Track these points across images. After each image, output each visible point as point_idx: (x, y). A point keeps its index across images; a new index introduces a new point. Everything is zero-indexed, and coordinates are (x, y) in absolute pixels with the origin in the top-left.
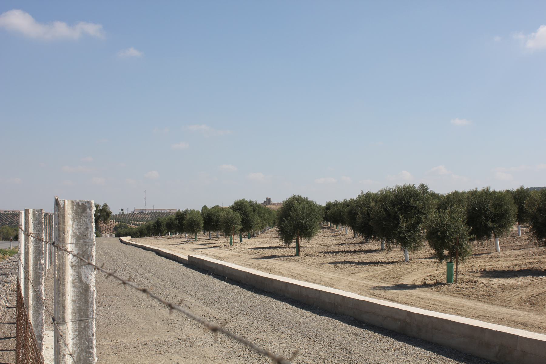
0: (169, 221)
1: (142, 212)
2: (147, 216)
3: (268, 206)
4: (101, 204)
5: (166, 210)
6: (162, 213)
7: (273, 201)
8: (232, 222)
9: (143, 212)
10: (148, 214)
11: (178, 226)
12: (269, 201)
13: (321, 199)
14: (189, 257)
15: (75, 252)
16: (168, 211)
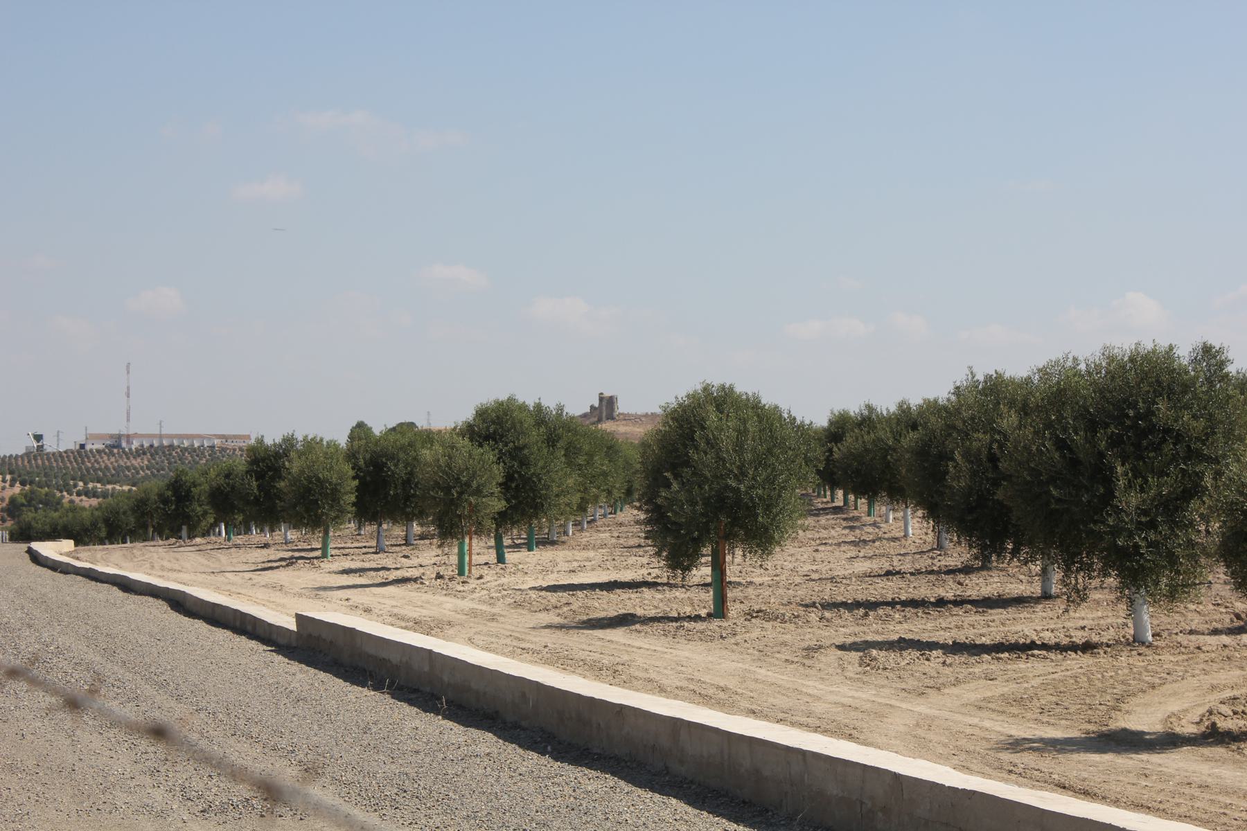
0: (221, 480)
1: (115, 444)
2: (136, 462)
3: (607, 426)
4: (607, 394)
5: (209, 437)
7: (622, 407)
9: (118, 446)
10: (141, 452)
14: (300, 618)
16: (217, 442)
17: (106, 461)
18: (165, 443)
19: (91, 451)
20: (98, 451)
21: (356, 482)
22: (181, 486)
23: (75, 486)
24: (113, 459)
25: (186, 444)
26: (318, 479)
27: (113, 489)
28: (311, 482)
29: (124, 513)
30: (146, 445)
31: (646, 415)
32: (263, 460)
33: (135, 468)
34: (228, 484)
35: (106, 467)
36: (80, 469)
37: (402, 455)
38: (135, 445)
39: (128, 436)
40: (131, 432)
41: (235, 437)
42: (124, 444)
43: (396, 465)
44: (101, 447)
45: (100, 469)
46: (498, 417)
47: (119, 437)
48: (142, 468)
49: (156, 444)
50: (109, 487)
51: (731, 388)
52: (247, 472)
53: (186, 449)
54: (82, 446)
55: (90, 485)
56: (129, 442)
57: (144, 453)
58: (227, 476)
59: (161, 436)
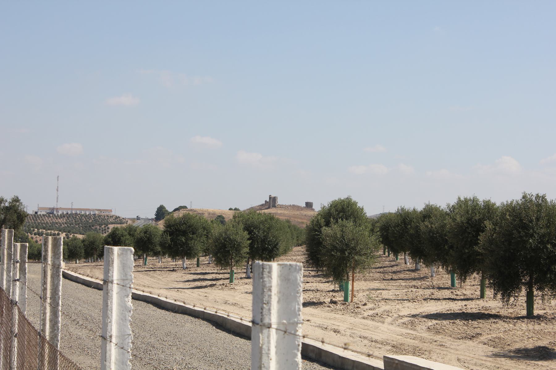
0: (142, 234)
1: (51, 212)
2: (60, 221)
3: (272, 211)
4: (273, 196)
5: (93, 210)
7: (280, 202)
8: (354, 249)
9: (53, 213)
10: (62, 216)
11: (170, 246)
12: (272, 202)
13: (377, 203)
14: (388, 362)
16: (97, 212)
17: (47, 220)
18: (74, 212)
19: (40, 215)
20: (43, 215)
21: (249, 242)
22: (116, 236)
23: (34, 230)
24: (50, 219)
25: (83, 213)
26: (230, 239)
27: (51, 232)
28: (225, 241)
29: (80, 247)
30: (65, 213)
32: (173, 226)
33: (60, 223)
34: (146, 237)
35: (47, 222)
36: (35, 223)
37: (261, 226)
38: (60, 213)
39: (57, 209)
40: (58, 207)
41: (105, 210)
42: (55, 212)
43: (258, 232)
44: (45, 213)
45: (44, 223)
46: (343, 208)
47: (53, 209)
48: (63, 223)
49: (69, 213)
50: (49, 231)
51: (543, 197)
52: (164, 232)
53: (83, 215)
54: (36, 213)
55: (40, 230)
57: (64, 217)
58: (145, 233)
59: (72, 209)
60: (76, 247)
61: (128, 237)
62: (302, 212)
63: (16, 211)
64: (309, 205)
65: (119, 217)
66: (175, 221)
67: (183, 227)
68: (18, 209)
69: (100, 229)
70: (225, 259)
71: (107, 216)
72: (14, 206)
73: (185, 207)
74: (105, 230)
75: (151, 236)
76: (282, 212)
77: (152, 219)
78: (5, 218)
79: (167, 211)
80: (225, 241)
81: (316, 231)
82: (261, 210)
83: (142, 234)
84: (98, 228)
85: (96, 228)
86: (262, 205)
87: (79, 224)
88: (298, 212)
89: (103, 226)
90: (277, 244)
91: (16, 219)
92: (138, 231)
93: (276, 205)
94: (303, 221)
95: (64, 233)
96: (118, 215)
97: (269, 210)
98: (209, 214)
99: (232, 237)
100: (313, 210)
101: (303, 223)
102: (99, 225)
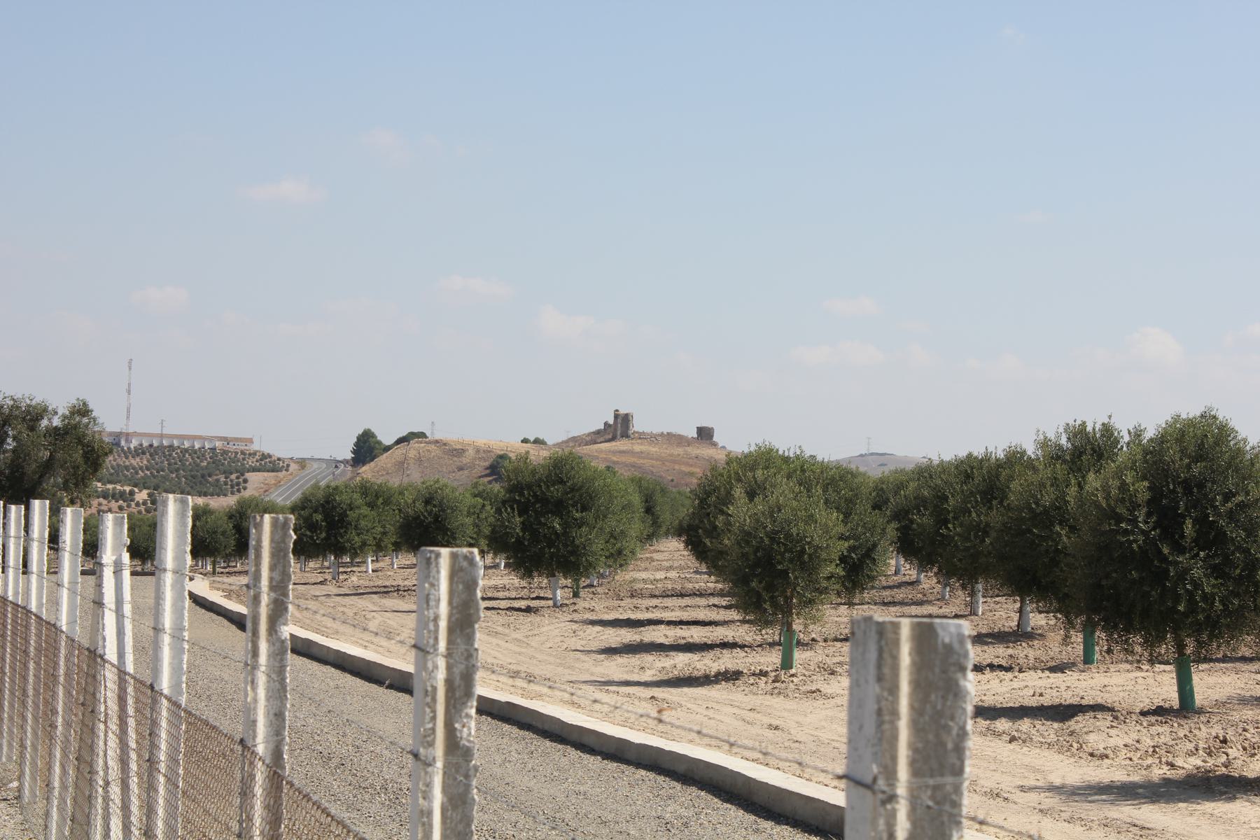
2: (135, 462)
4: (623, 411)
5: (211, 439)
6: (191, 451)
7: (638, 426)
9: (118, 444)
10: (140, 451)
11: (519, 541)
12: (620, 426)
15: (267, 761)
16: (218, 444)
18: (165, 443)
22: (334, 508)
25: (187, 445)
26: (788, 536)
29: (223, 533)
30: (145, 444)
31: (662, 434)
32: (529, 487)
34: (430, 513)
38: (134, 443)
39: (127, 434)
40: (131, 431)
42: (123, 443)
48: (141, 468)
49: (156, 444)
50: (110, 486)
53: (186, 450)
56: (127, 441)
57: (144, 453)
58: (428, 502)
59: (162, 436)
60: (215, 532)
61: (365, 510)
62: (689, 449)
63: (80, 441)
64: (705, 434)
65: (270, 456)
66: (534, 472)
67: (556, 492)
68: (84, 435)
69: (226, 484)
70: (772, 598)
71: (243, 453)
72: (76, 427)
73: (422, 435)
74: (238, 484)
75: (443, 511)
76: (643, 448)
77: (345, 462)
78: (51, 457)
79: (379, 443)
80: (772, 539)
81: (1119, 519)
82: (596, 443)
83: (420, 506)
84: (223, 479)
85: (218, 481)
86: (598, 432)
87: (177, 470)
88: (680, 451)
89: (233, 477)
90: (875, 546)
91: (80, 460)
92: (409, 498)
93: (630, 432)
94: (686, 473)
95: (145, 492)
96: (267, 451)
97: (614, 443)
98: (478, 451)
99: (794, 531)
100: (715, 445)
101: (692, 474)
102: (225, 472)
